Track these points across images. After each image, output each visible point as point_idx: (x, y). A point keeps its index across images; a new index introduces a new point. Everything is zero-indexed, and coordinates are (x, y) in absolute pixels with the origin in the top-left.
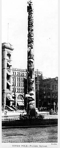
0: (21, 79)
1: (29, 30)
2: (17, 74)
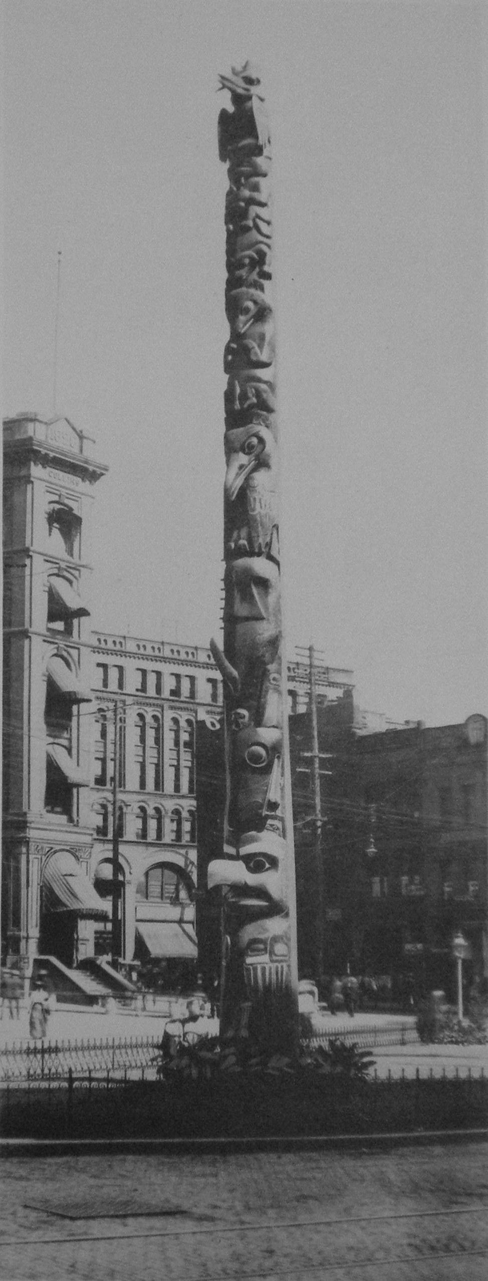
0: (168, 724)
1: (233, 308)
2: (133, 682)
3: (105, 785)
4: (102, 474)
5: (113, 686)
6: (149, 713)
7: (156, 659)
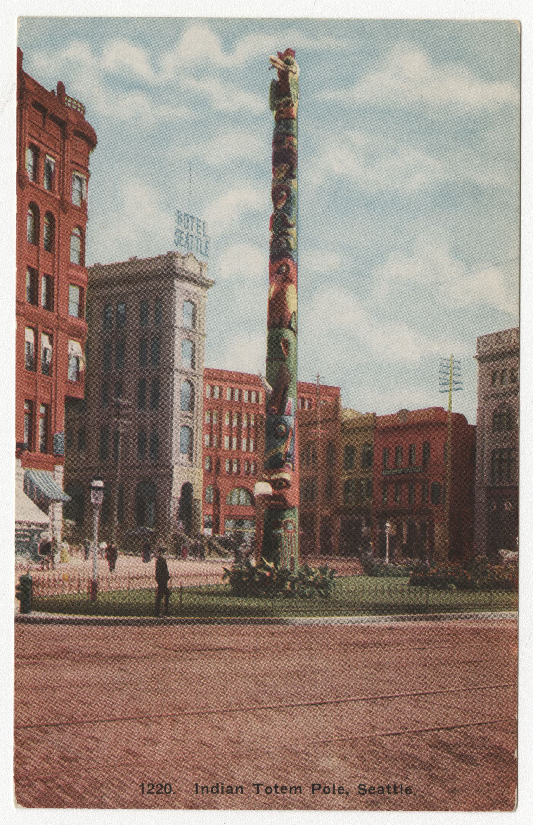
4: (212, 286)
5: (236, 398)
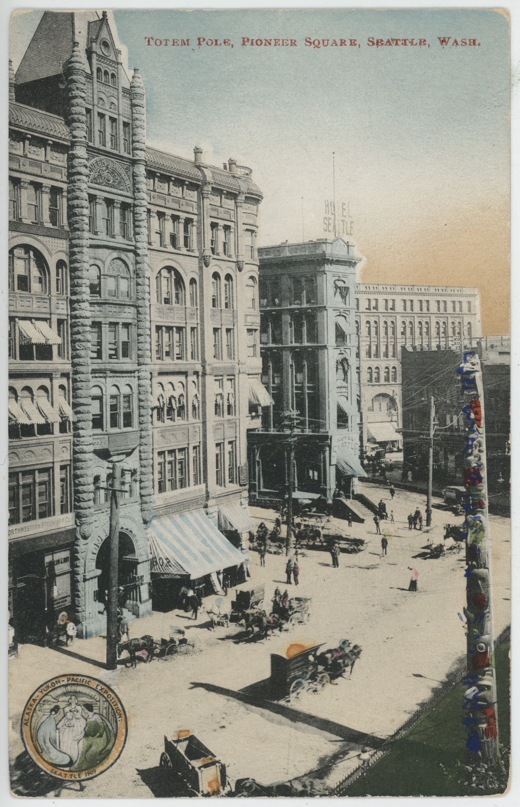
3: (51, 358)
6: (424, 320)
7: (374, 293)
